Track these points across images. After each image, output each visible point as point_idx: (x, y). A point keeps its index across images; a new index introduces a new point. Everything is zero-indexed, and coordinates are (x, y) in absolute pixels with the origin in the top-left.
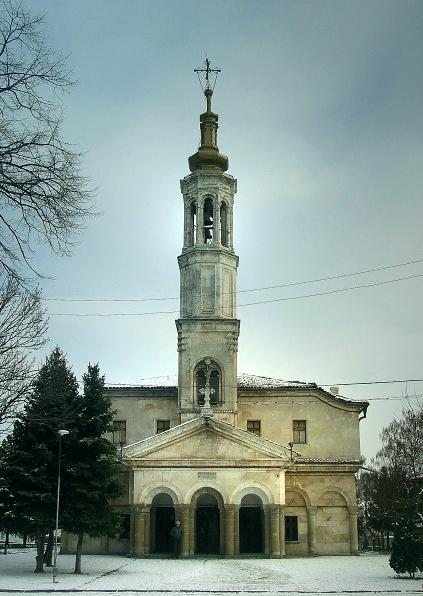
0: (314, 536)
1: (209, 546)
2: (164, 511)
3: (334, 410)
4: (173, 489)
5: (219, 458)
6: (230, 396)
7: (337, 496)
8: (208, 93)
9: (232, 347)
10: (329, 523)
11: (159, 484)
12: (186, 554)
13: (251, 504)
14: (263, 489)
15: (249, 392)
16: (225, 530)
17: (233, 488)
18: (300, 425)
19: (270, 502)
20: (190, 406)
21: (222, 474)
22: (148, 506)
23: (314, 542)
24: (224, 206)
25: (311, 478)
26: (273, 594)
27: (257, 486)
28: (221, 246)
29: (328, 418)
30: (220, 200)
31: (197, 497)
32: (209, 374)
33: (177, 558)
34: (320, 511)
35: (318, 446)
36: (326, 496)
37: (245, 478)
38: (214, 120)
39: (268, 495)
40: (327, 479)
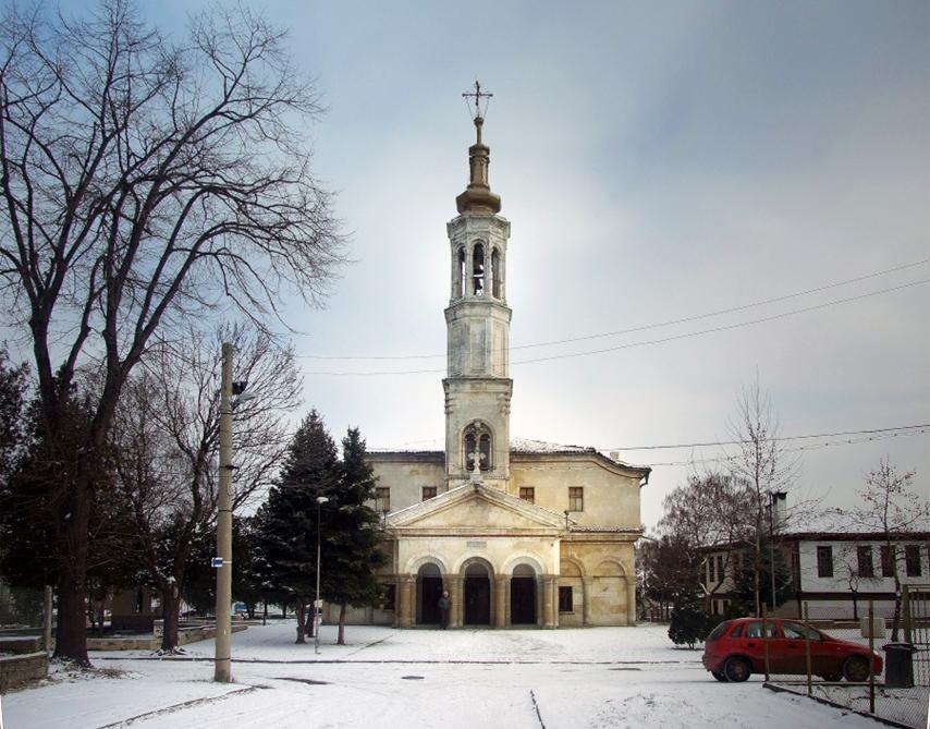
1: (478, 615)
2: (431, 583)
3: (614, 476)
4: (440, 558)
5: (489, 527)
6: (501, 461)
7: (615, 566)
8: (478, 122)
9: (503, 408)
10: (607, 593)
13: (431, 574)
17: (505, 558)
18: (577, 492)
19: (544, 572)
20: (458, 472)
21: (491, 542)
22: (414, 576)
23: (590, 613)
24: (496, 253)
27: (530, 555)
29: (607, 485)
30: (491, 246)
34: (596, 582)
37: (517, 547)
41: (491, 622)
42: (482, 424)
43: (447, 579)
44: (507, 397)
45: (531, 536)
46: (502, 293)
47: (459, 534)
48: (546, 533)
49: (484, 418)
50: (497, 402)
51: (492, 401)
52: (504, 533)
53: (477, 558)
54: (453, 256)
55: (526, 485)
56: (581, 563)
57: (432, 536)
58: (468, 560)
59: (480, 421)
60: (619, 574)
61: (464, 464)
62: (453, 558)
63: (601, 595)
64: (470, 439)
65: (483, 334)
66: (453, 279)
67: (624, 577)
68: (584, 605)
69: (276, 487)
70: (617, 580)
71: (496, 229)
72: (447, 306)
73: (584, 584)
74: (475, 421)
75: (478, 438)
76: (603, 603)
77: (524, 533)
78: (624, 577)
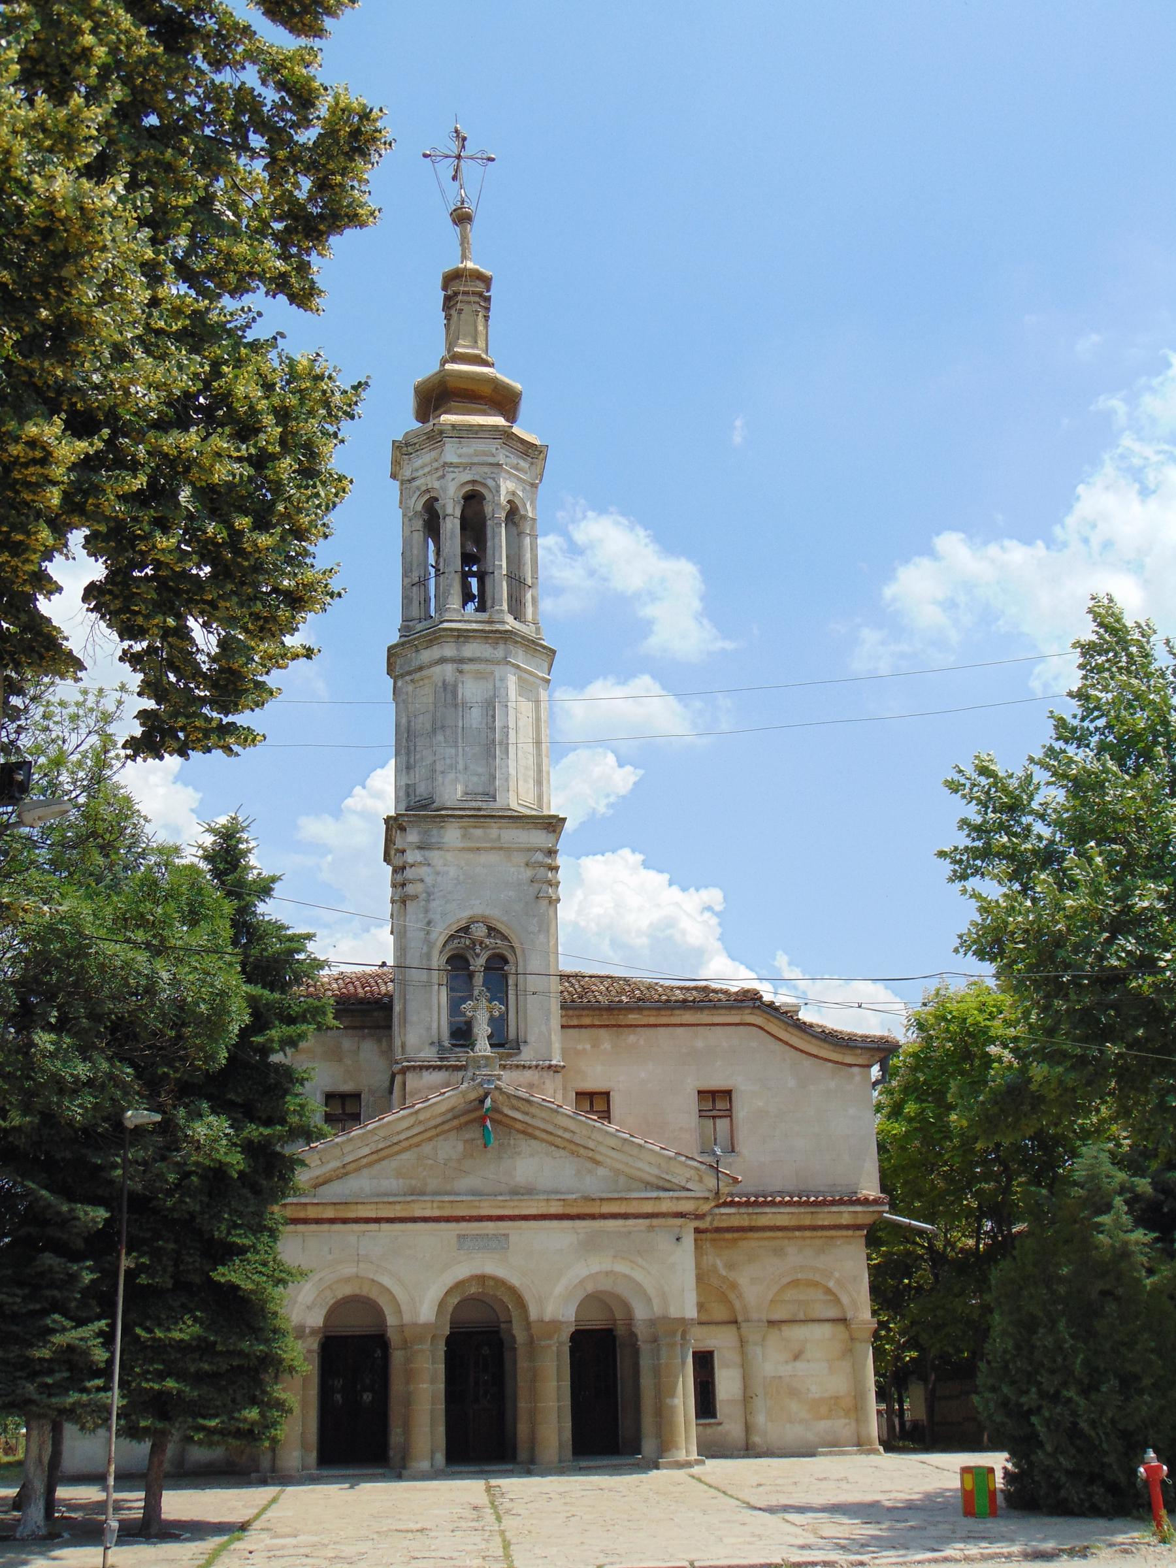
0: (759, 1404)
1: (484, 1440)
2: (357, 1355)
3: (808, 1062)
4: (386, 1281)
5: (515, 1192)
6: (543, 1027)
7: (820, 1295)
8: (461, 218)
9: (542, 890)
10: (799, 1365)
11: (349, 1270)
12: (425, 1465)
13: (356, 1324)
14: (638, 1276)
15: (606, 1008)
16: (534, 1395)
17: (553, 1279)
18: (716, 1102)
19: (658, 1310)
20: (429, 1054)
21: (522, 1235)
22: (314, 1332)
23: (760, 1419)
24: (513, 515)
25: (752, 1243)
26: (635, 1565)
27: (622, 1268)
28: (509, 619)
29: (792, 1083)
30: (503, 500)
31: (455, 1300)
32: (481, 964)
33: (399, 1477)
34: (774, 1335)
35: (965, 1123)
36: (790, 1294)
37: (590, 1245)
38: (480, 287)
39: (651, 1291)
40: (791, 1249)
41: (522, 1455)
42: (491, 930)
43: (406, 1345)
44: (399, 878)
45: (625, 1216)
46: (529, 611)
47: (436, 1213)
48: (665, 1207)
49: (496, 914)
50: (529, 873)
51: (516, 870)
52: (555, 1209)
53: (482, 1279)
54: (407, 519)
55: (590, 1085)
56: (734, 1286)
57: (368, 1221)
58: (459, 1285)
59: (484, 920)
60: (832, 1313)
61: (445, 1033)
62: (418, 1282)
63: (785, 1370)
64: (458, 963)
65: (489, 706)
66: (406, 574)
67: (843, 1321)
68: (747, 1399)
69: (974, 948)
70: (826, 1330)
71: (514, 460)
72: (395, 639)
73: (742, 1342)
74: (473, 921)
75: (479, 963)
76: (793, 1393)
77: (606, 1209)
78: (843, 1321)
